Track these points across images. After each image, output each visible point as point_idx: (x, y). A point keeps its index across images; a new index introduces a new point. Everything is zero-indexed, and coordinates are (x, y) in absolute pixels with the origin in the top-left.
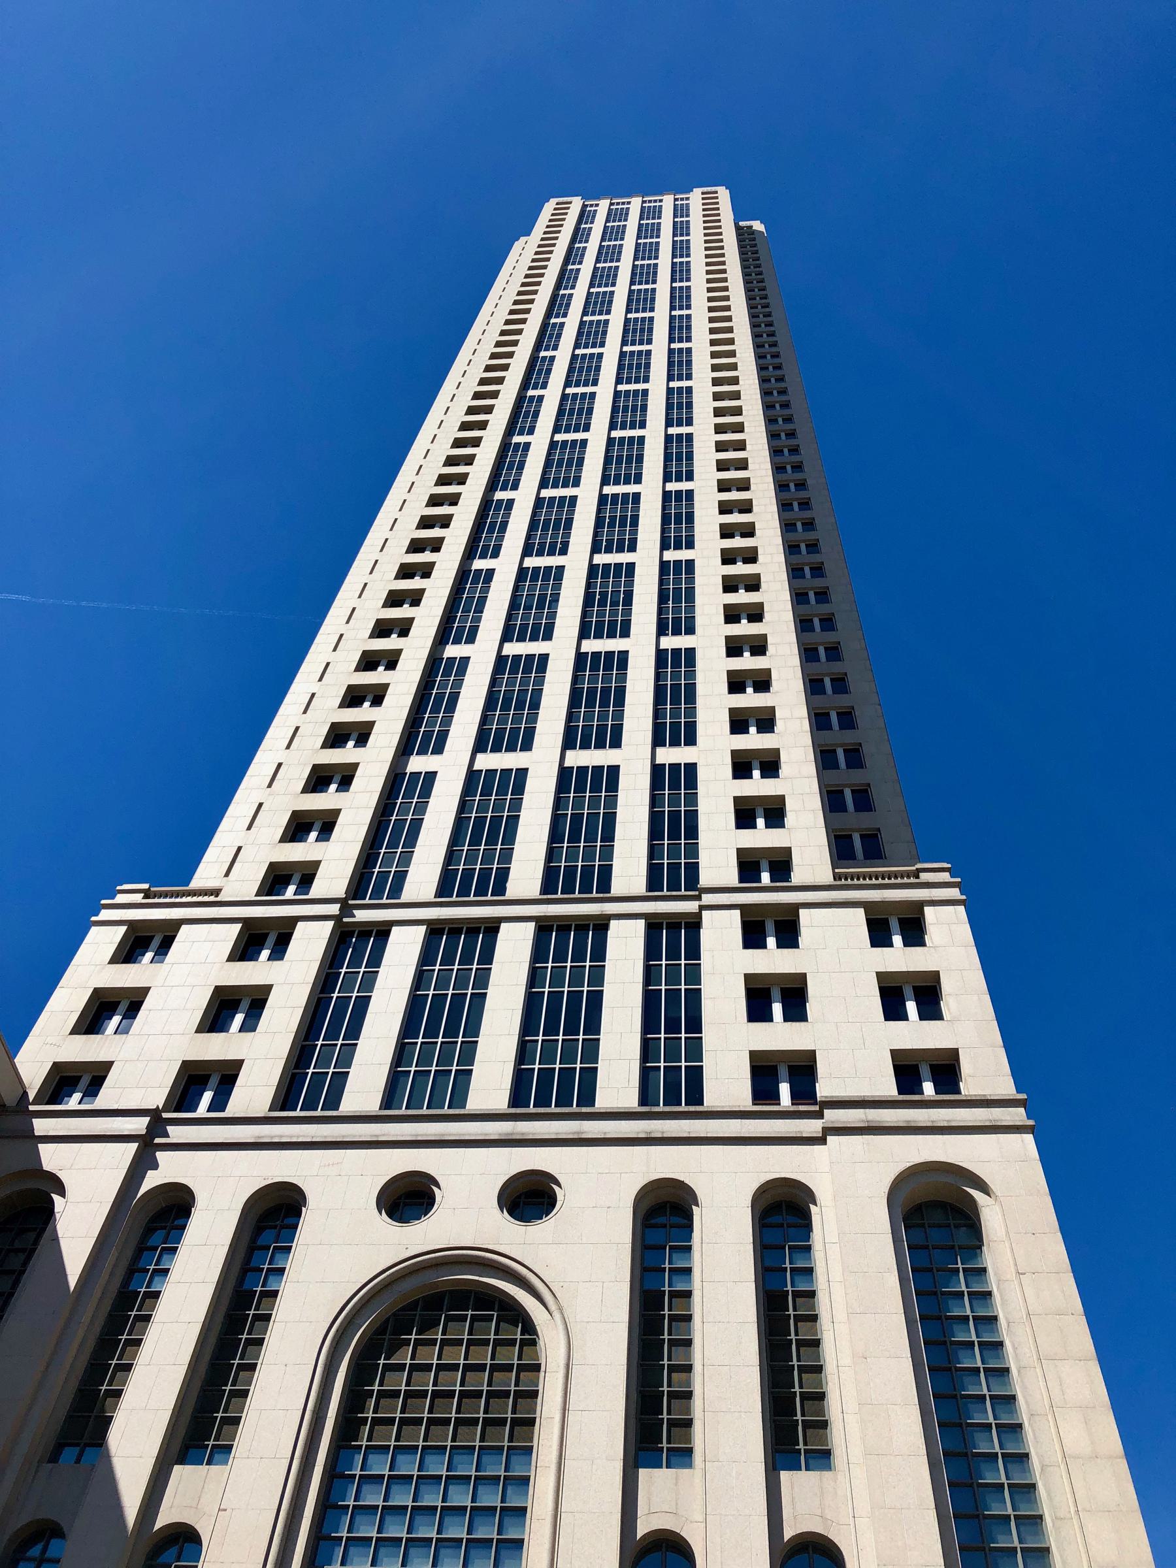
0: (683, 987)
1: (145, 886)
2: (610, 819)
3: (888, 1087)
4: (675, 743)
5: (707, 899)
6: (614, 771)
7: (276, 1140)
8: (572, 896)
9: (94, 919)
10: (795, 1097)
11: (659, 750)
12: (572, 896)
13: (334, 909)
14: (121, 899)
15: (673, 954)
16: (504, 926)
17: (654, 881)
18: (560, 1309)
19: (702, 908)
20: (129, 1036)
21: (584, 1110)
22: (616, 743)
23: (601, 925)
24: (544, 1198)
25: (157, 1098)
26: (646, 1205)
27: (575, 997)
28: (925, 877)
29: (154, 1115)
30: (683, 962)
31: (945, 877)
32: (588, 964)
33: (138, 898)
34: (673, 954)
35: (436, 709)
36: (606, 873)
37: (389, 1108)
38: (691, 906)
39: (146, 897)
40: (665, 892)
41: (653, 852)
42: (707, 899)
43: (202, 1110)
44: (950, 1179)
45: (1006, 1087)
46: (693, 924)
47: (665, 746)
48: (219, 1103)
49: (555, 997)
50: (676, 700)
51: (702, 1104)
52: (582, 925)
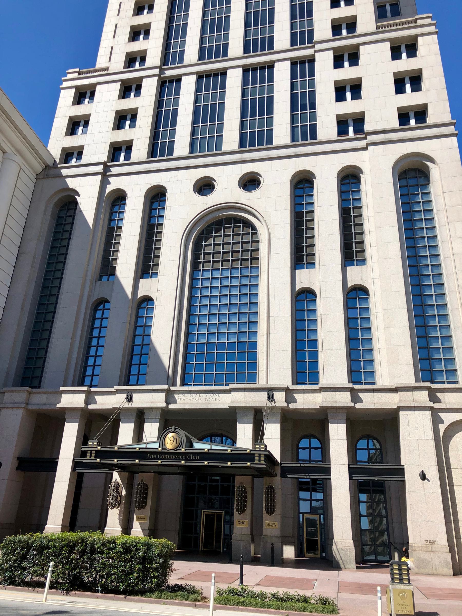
5: (318, 47)
9: (61, 87)
10: (355, 132)
14: (70, 76)
16: (229, 71)
18: (265, 221)
19: (315, 52)
25: (104, 157)
28: (419, 22)
31: (429, 21)
33: (76, 75)
34: (303, 76)
37: (193, 153)
38: (310, 52)
39: (79, 74)
42: (318, 47)
48: (128, 157)
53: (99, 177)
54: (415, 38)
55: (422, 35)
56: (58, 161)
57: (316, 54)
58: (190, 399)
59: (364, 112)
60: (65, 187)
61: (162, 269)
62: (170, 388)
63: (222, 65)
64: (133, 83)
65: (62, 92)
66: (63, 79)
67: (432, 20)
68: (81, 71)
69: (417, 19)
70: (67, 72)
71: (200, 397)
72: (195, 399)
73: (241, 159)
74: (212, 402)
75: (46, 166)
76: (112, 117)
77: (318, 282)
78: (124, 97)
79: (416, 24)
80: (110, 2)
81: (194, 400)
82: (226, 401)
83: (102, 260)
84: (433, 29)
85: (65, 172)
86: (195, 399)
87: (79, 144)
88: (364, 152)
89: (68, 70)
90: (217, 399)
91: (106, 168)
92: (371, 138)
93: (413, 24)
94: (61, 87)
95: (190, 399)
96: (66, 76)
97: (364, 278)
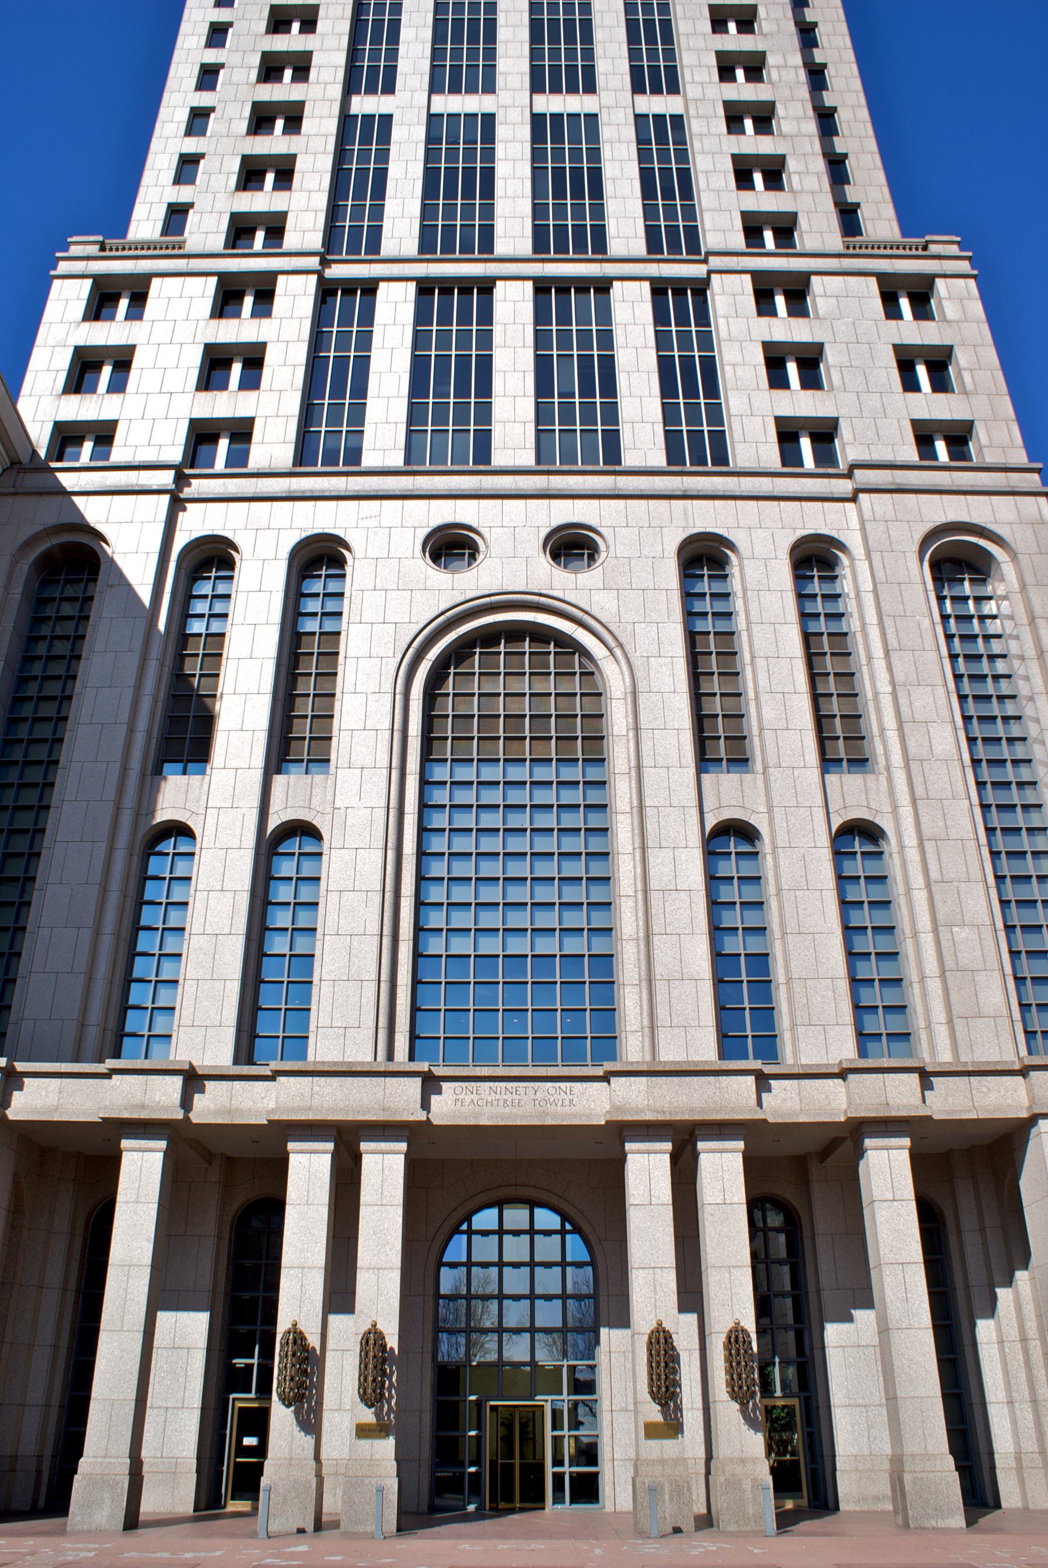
0: (454, 353)
1: (100, 238)
2: (381, 176)
3: (910, 453)
4: (371, 90)
5: (715, 262)
6: (387, 120)
7: (327, 494)
8: (659, 257)
9: (52, 273)
10: (818, 460)
11: (435, 98)
12: (659, 257)
13: (314, 262)
15: (682, 320)
16: (382, 286)
17: (426, 244)
18: (621, 646)
19: (710, 272)
20: (263, 394)
21: (482, 468)
22: (389, 88)
23: (486, 287)
24: (583, 549)
25: (175, 454)
26: (304, 555)
27: (463, 362)
28: (934, 249)
29: (178, 469)
30: (435, 328)
31: (954, 250)
32: (435, 328)
33: (94, 250)
34: (682, 320)
35: (376, 40)
36: (376, 234)
39: (103, 249)
40: (439, 255)
41: (427, 211)
42: (715, 262)
43: (220, 465)
44: (439, 534)
45: (1020, 458)
46: (701, 288)
47: (478, 92)
48: (238, 458)
49: (443, 361)
50: (651, 40)
51: (489, 463)
52: (465, 286)
53: (166, 499)
54: (929, 280)
55: (945, 276)
56: (42, 453)
57: (713, 276)
58: (490, 1099)
59: (837, 419)
60: (67, 519)
61: (340, 748)
62: (13, 1067)
63: (483, 271)
64: (249, 287)
65: (56, 283)
66: (58, 255)
67: (961, 250)
68: (107, 241)
69: (928, 243)
70: (69, 240)
71: (518, 1097)
72: (505, 1101)
73: (548, 490)
74: (552, 1109)
75: (12, 464)
76: (194, 358)
77: (763, 809)
78: (245, 189)
79: (924, 253)
80: (188, 4)
81: (501, 1103)
82: (593, 1106)
83: (260, 134)
84: (964, 266)
85: (68, 480)
86: (505, 1101)
87: (105, 416)
88: (106, 1081)
89: (71, 237)
90: (567, 1103)
91: (182, 479)
92: (862, 476)
93: (920, 252)
94: (52, 273)
95: (490, 1099)
96: (67, 250)
97: (873, 805)
